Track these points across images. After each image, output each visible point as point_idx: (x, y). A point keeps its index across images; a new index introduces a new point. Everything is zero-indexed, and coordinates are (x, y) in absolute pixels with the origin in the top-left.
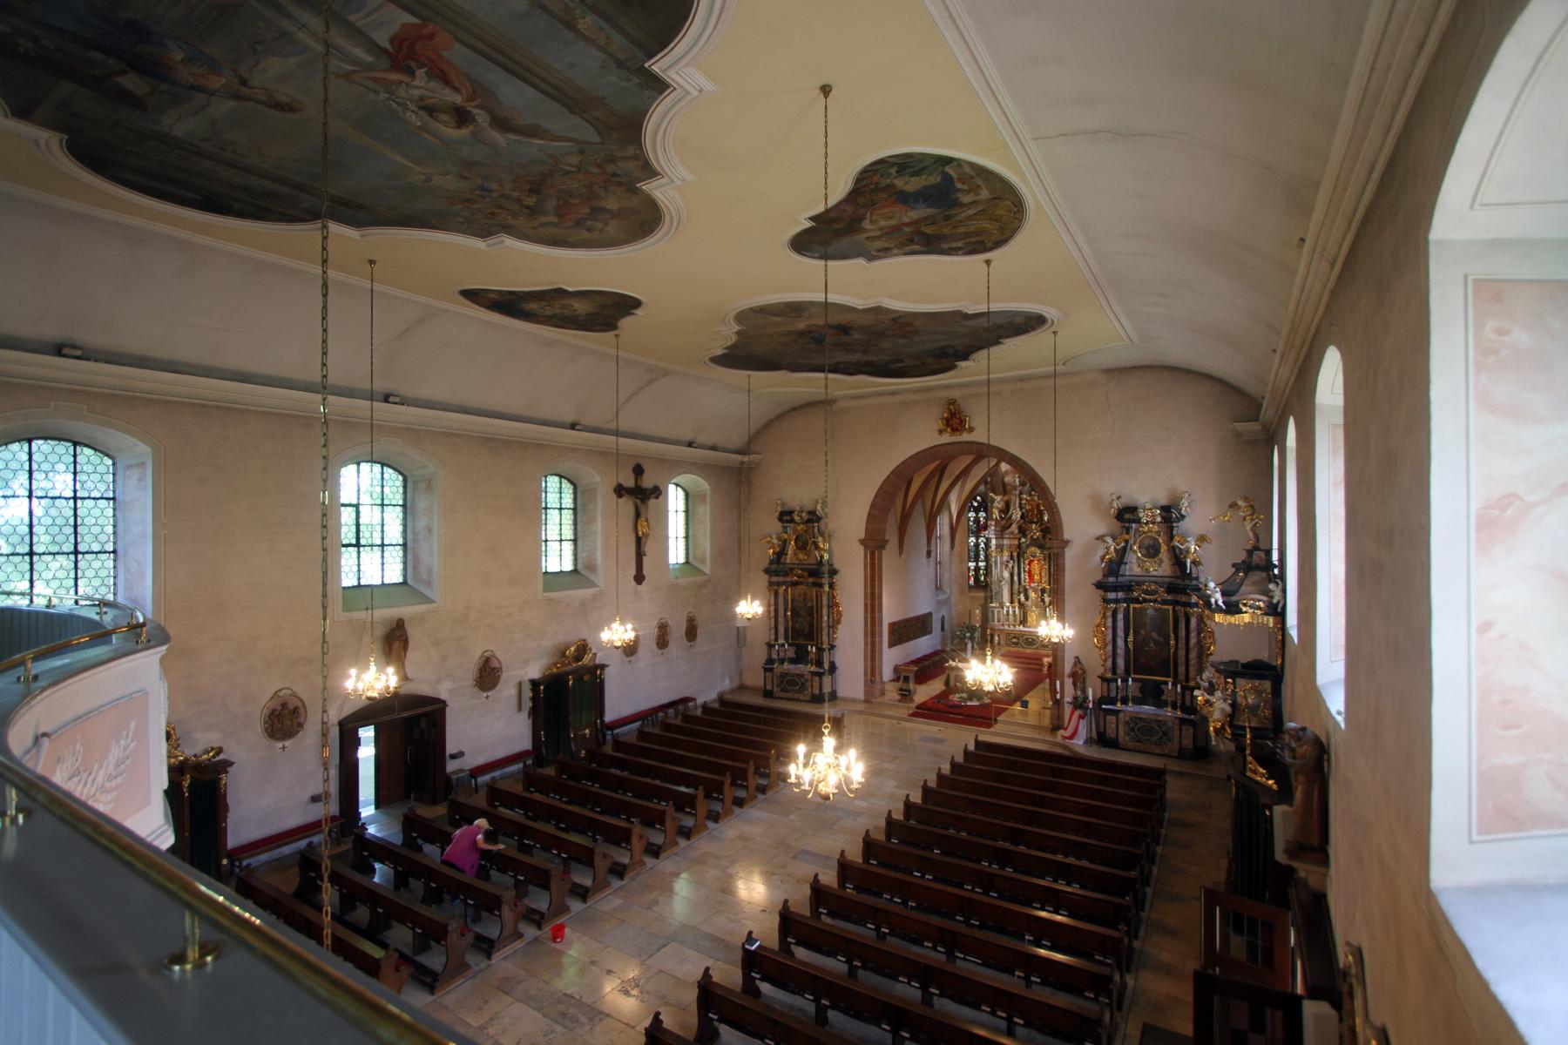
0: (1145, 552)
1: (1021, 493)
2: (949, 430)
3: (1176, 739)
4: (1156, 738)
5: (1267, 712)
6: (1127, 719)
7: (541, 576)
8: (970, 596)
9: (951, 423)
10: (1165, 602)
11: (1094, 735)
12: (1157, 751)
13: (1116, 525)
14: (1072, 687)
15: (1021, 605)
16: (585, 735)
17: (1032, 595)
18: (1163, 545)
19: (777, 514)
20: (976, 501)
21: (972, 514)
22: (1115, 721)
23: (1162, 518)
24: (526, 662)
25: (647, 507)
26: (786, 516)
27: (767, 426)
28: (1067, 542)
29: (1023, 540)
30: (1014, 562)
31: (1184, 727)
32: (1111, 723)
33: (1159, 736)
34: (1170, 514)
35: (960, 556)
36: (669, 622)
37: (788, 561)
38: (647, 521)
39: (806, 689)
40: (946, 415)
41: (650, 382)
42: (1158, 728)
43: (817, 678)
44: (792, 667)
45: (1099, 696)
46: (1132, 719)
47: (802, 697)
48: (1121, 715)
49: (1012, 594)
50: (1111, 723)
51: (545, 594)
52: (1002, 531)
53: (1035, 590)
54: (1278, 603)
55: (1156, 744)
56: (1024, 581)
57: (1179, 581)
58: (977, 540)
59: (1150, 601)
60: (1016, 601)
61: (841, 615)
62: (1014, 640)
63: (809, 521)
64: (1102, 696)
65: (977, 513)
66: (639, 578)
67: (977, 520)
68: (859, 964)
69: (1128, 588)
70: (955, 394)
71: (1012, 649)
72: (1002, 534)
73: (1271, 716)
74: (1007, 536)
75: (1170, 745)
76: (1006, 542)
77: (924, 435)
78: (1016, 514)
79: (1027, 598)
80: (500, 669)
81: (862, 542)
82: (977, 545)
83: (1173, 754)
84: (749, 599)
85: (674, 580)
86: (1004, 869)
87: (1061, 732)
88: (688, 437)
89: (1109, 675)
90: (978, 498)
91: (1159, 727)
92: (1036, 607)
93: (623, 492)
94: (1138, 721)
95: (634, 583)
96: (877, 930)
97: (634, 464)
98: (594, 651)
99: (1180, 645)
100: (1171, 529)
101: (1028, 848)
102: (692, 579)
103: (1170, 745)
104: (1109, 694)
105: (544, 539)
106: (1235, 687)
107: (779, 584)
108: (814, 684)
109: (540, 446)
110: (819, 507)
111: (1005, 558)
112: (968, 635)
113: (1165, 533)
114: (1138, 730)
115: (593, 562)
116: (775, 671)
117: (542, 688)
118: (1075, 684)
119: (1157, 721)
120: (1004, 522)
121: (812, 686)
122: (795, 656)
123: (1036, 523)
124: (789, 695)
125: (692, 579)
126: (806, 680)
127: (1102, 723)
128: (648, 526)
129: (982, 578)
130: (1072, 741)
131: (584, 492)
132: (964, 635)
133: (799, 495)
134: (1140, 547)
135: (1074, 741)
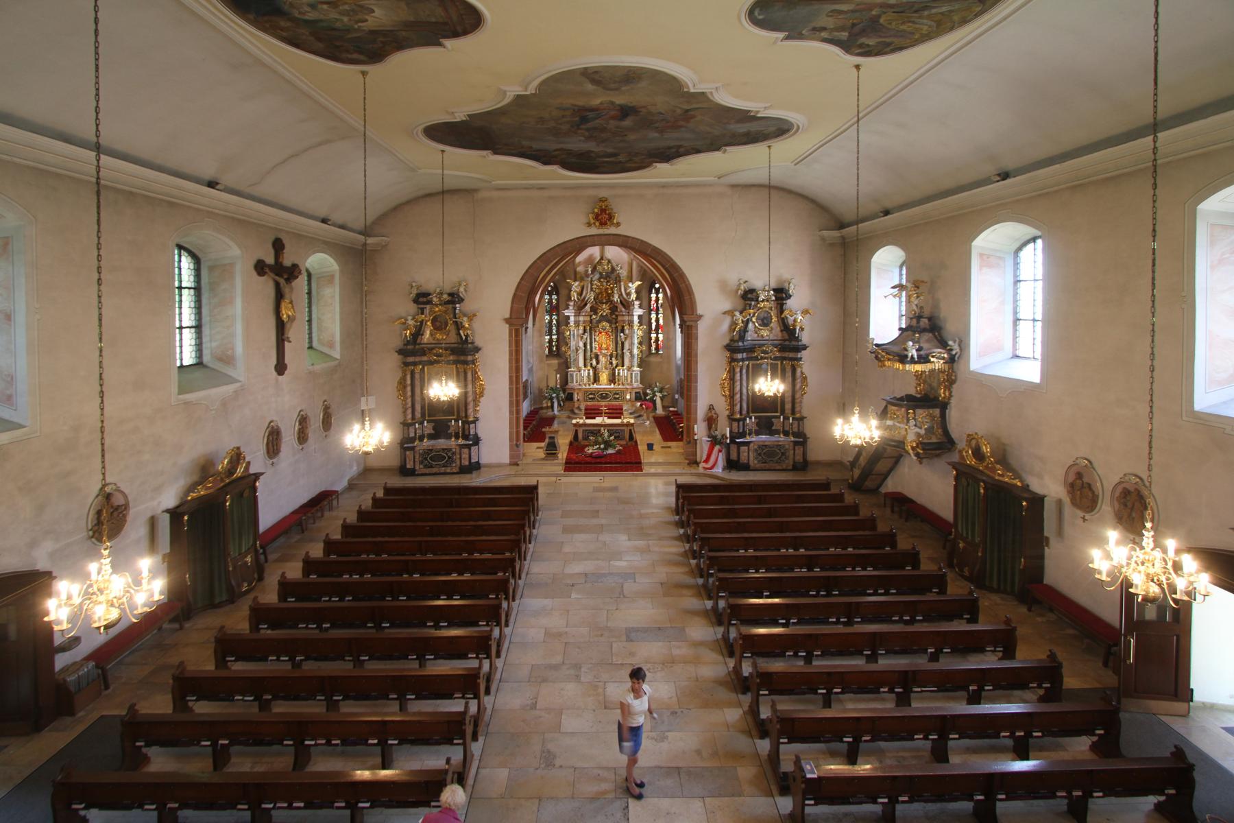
0: (760, 322)
2: (597, 224)
3: (791, 456)
4: (776, 458)
5: (940, 431)
6: (756, 447)
7: (175, 374)
8: (548, 364)
9: (600, 217)
10: (776, 358)
12: (778, 467)
13: (740, 304)
15: (595, 369)
16: (246, 562)
17: (602, 359)
18: (773, 317)
19: (413, 295)
20: (551, 286)
21: (547, 297)
23: (775, 296)
24: (158, 489)
25: (292, 289)
26: (422, 299)
27: (397, 209)
28: (701, 316)
29: (594, 317)
31: (797, 448)
33: (780, 456)
34: (781, 294)
35: (540, 331)
36: (309, 414)
37: (425, 341)
38: (291, 302)
39: (453, 461)
40: (596, 210)
41: (327, 142)
42: (778, 451)
43: (466, 451)
44: (432, 442)
46: (759, 447)
47: (448, 470)
48: (752, 445)
49: (585, 359)
50: (744, 452)
51: (181, 397)
52: (580, 308)
53: (605, 355)
54: (956, 354)
55: (777, 462)
56: (595, 349)
57: (787, 343)
58: (551, 317)
59: (765, 358)
61: (483, 389)
62: (618, 396)
63: (448, 302)
65: (550, 296)
66: (281, 368)
67: (550, 301)
68: (270, 697)
69: (751, 349)
70: (603, 193)
71: (589, 403)
72: (580, 313)
73: (942, 433)
75: (787, 461)
76: (581, 319)
77: (573, 226)
78: (591, 296)
79: (598, 363)
80: (126, 506)
81: (507, 321)
82: (551, 321)
84: (769, 377)
85: (311, 368)
86: (308, 577)
88: (323, 213)
90: (552, 284)
92: (606, 368)
93: (267, 270)
94: (764, 447)
95: (275, 373)
96: (292, 659)
97: (273, 238)
98: (247, 459)
100: (782, 305)
101: (434, 555)
102: (324, 365)
105: (178, 325)
106: (915, 416)
107: (415, 364)
108: (463, 456)
109: (171, 205)
110: (462, 289)
112: (554, 395)
114: (764, 453)
115: (229, 353)
116: (417, 449)
117: (186, 518)
119: (777, 445)
121: (461, 458)
122: (433, 432)
123: (606, 303)
124: (435, 470)
125: (324, 365)
126: (454, 454)
128: (293, 307)
129: (555, 349)
131: (211, 269)
132: (551, 396)
133: (433, 278)
134: (757, 319)
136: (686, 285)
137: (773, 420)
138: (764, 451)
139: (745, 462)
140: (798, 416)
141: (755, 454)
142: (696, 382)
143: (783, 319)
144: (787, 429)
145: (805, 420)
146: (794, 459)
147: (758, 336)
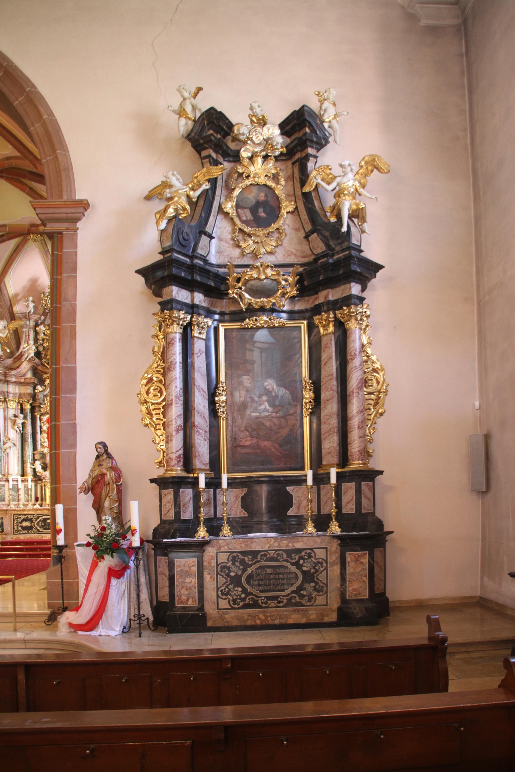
0: (247, 215)
1: (37, 325)
3: (335, 584)
6: (223, 558)
11: (147, 611)
12: (294, 618)
14: (93, 513)
22: (195, 569)
28: (84, 205)
29: (39, 388)
30: (25, 417)
31: (349, 556)
32: (188, 574)
42: (294, 569)
45: (155, 522)
50: (188, 574)
55: (289, 604)
59: (262, 310)
60: (29, 470)
62: (25, 524)
64: (163, 522)
74: (14, 380)
75: (320, 600)
83: (326, 619)
87: (69, 617)
89: (178, 471)
91: (297, 564)
99: (324, 395)
103: (320, 600)
104: (177, 514)
111: (11, 413)
113: (290, 178)
114: (250, 578)
118: (98, 507)
120: (9, 361)
127: (164, 582)
130: (94, 633)
135: (100, 631)
136: (44, 125)
137: (289, 489)
138: (249, 571)
139: (190, 603)
140: (356, 465)
141: (222, 580)
142: (73, 389)
143: (306, 196)
144: (325, 511)
145: (379, 478)
146: (343, 595)
147: (243, 255)
